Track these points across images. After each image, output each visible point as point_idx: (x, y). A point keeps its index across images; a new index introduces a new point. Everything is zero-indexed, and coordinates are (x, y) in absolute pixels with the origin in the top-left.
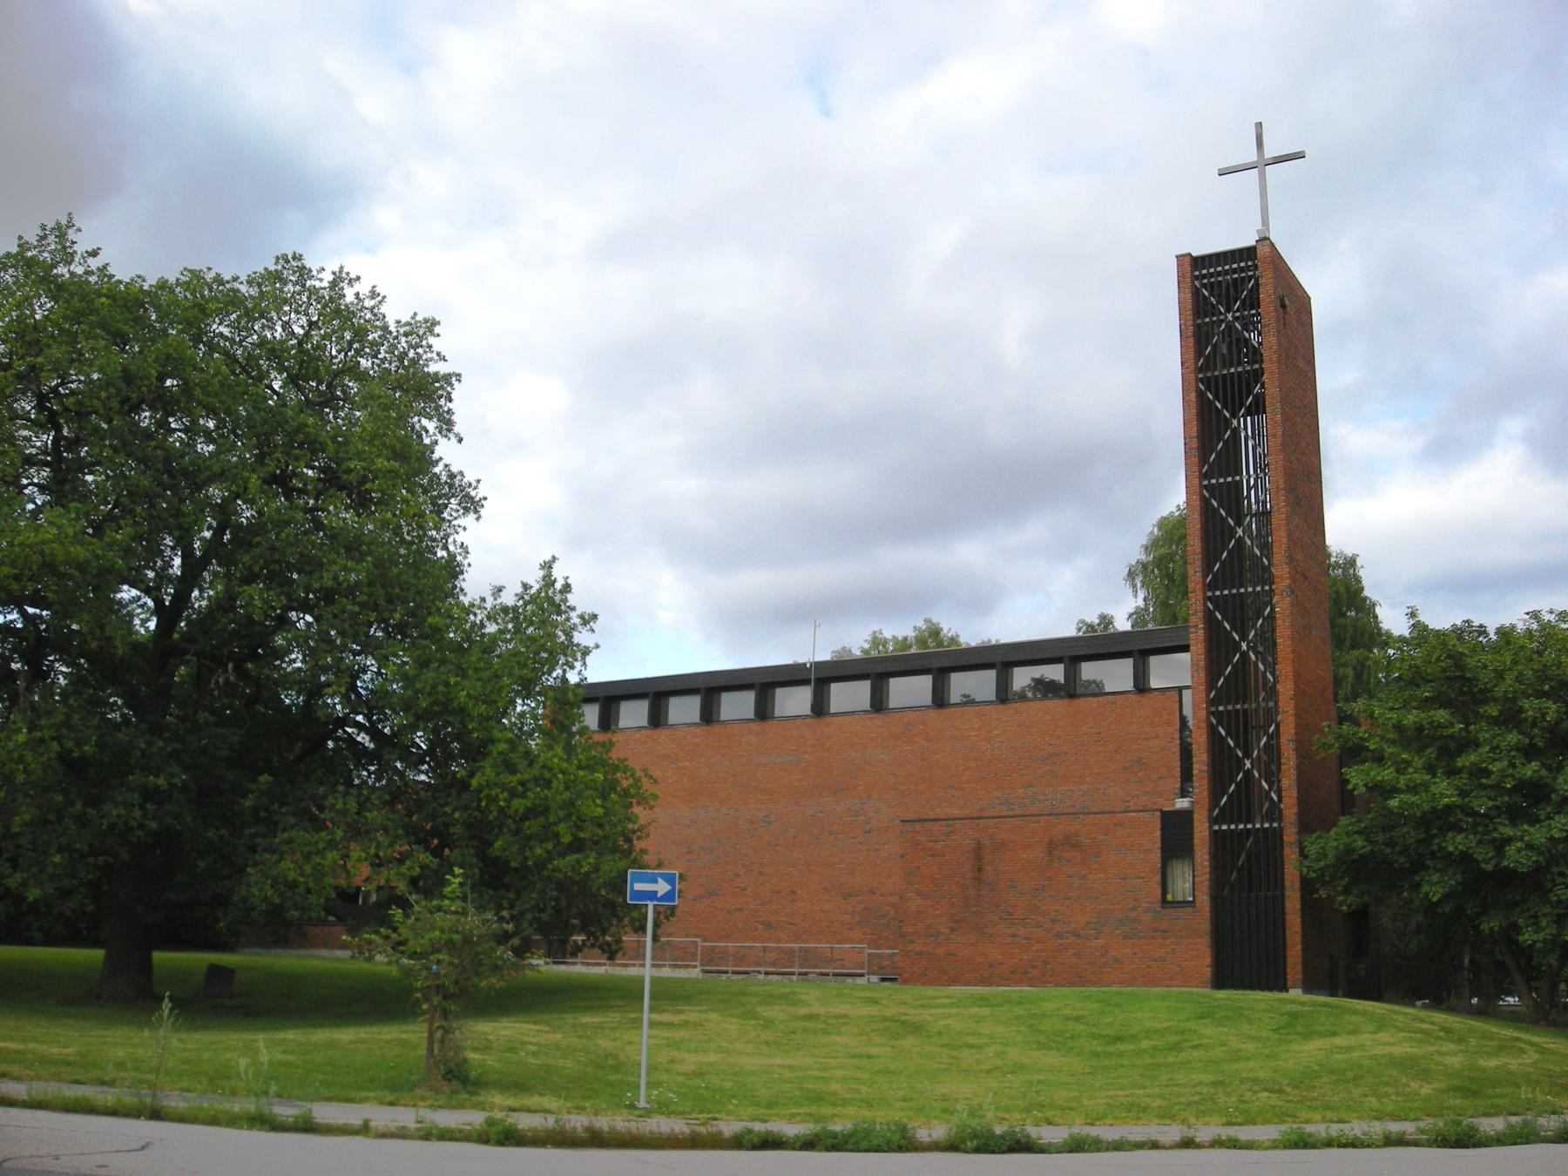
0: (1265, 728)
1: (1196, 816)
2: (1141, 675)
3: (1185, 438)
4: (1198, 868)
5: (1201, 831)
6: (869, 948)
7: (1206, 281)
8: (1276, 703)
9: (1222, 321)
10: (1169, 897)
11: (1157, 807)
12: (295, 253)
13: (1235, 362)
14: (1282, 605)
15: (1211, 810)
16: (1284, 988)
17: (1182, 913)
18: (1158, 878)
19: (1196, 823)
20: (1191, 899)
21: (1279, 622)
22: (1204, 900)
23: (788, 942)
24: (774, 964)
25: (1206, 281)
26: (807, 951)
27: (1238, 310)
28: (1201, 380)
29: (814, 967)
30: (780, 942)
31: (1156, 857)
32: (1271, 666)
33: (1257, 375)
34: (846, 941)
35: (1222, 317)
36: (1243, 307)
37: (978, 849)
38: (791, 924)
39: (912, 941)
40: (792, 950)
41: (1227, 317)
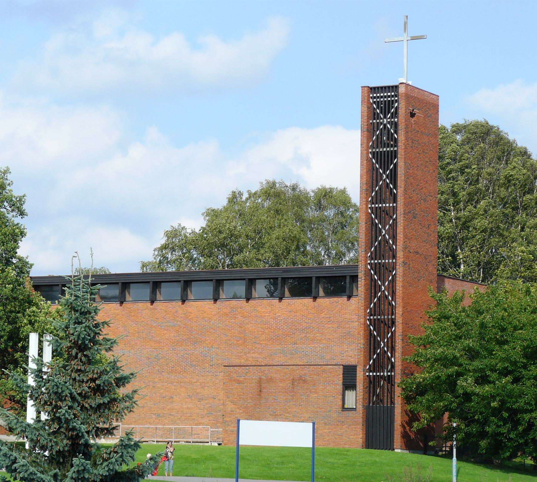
0: (391, 272)
1: (358, 368)
2: (348, 410)
3: (361, 184)
4: (358, 392)
5: (360, 375)
6: (211, 428)
7: (375, 100)
8: (397, 205)
9: (381, 124)
10: (346, 406)
11: (341, 363)
12: (140, 448)
13: (390, 312)
14: (399, 271)
15: (365, 366)
16: (391, 448)
17: (350, 413)
18: (341, 397)
19: (358, 372)
20: (355, 407)
21: (398, 279)
22: (360, 408)
23: (168, 424)
24: (162, 437)
25: (375, 100)
26: (179, 429)
27: (389, 118)
28: (371, 208)
29: (183, 438)
30: (164, 425)
31: (340, 387)
32: (395, 242)
33: (395, 154)
34: (200, 424)
35: (381, 121)
36: (392, 117)
37: (260, 381)
38: (170, 415)
39: (228, 425)
40: (171, 429)
41: (383, 121)
